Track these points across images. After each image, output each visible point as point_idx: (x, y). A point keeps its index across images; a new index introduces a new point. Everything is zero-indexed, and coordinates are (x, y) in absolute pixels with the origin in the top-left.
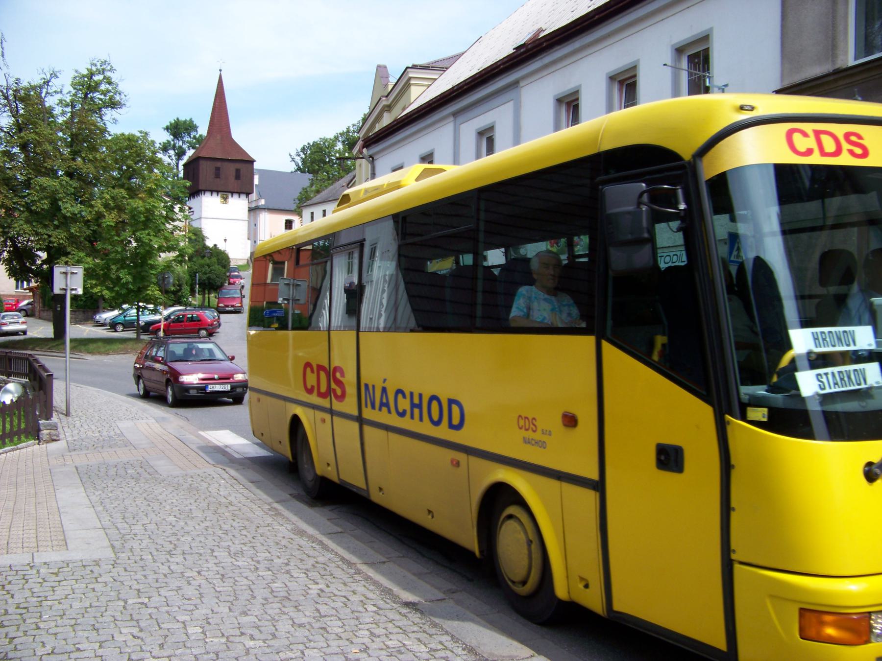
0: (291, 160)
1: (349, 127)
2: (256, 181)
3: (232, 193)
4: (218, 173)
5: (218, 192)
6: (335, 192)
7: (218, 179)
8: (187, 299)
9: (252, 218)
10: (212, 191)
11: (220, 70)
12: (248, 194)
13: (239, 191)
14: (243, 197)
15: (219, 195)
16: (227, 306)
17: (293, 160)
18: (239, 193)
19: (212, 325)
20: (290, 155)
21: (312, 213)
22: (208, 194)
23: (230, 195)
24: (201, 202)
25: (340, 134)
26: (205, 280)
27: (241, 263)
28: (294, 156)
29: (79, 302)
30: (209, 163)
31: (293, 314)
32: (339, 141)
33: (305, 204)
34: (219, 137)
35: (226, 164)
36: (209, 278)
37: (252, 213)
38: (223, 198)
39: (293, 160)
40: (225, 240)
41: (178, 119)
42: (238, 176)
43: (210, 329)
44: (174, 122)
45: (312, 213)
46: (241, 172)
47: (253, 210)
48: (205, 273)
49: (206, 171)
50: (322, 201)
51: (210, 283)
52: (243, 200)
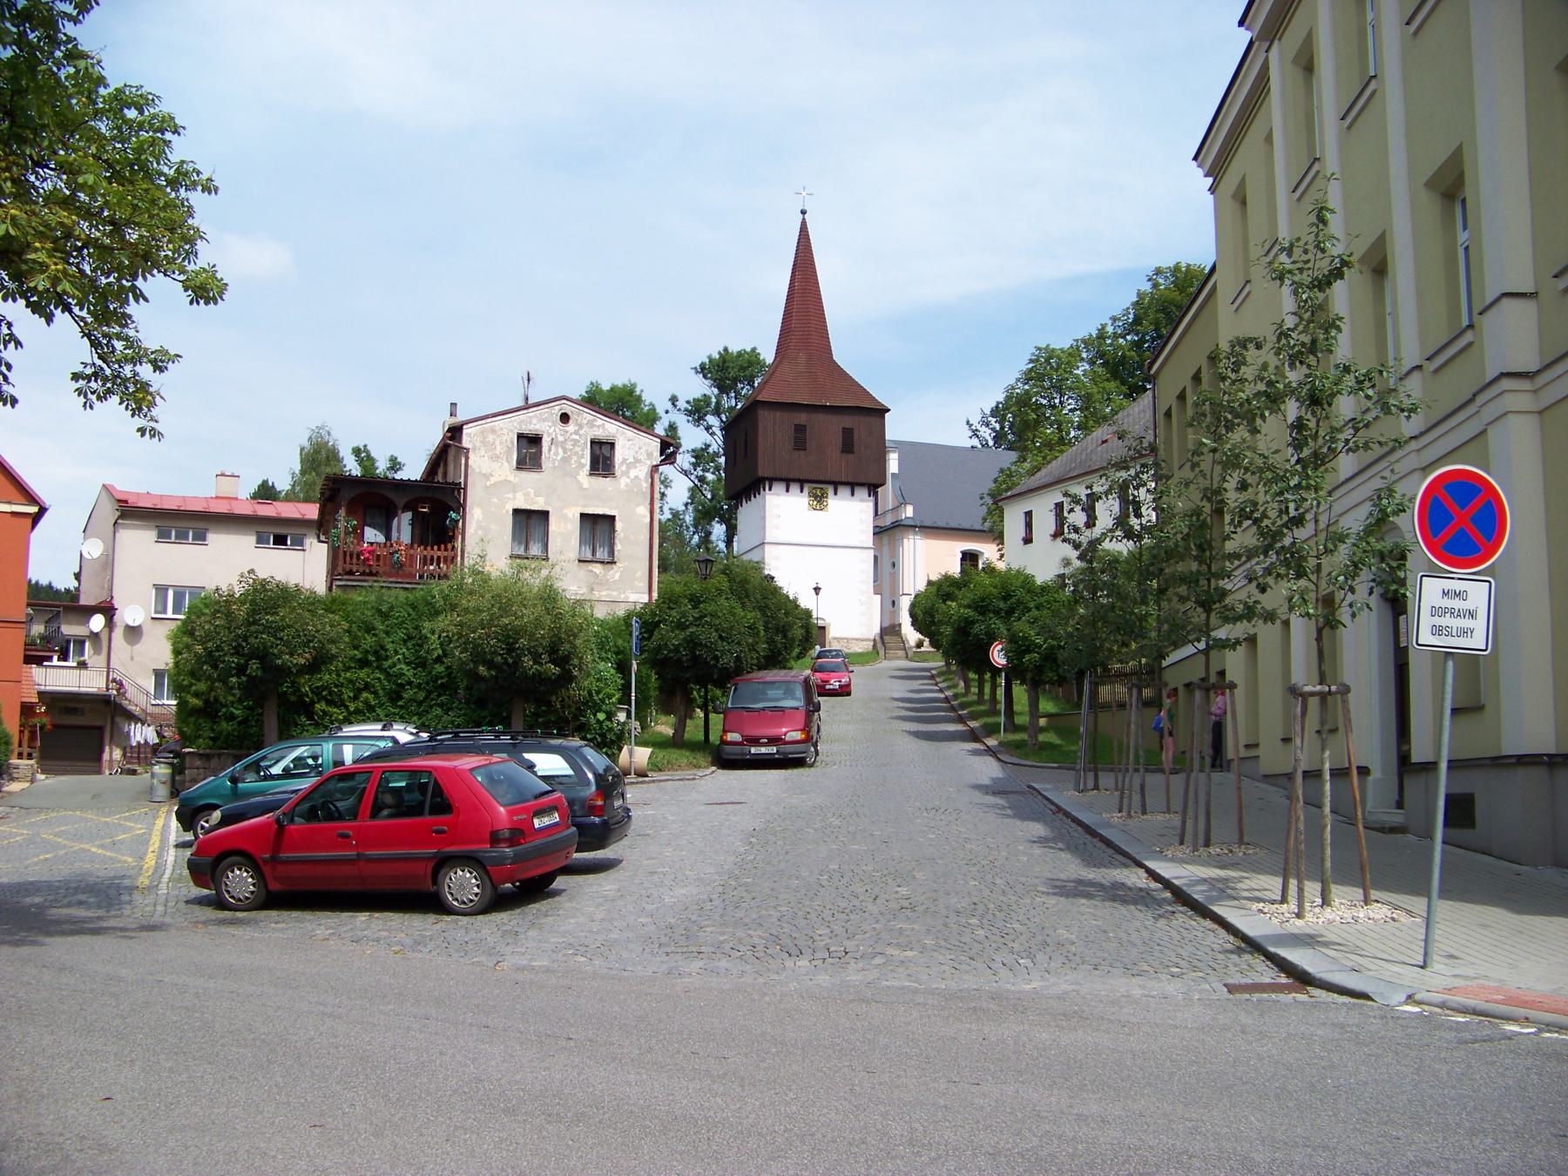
0: (970, 434)
1: (1104, 326)
2: (893, 465)
3: (836, 485)
4: (800, 438)
5: (802, 483)
6: (1084, 457)
7: (802, 453)
8: (610, 716)
9: (886, 549)
10: (788, 482)
11: (803, 212)
12: (873, 488)
13: (850, 480)
14: (862, 493)
15: (806, 490)
16: (755, 741)
17: (975, 433)
18: (853, 486)
19: (520, 833)
20: (968, 423)
21: (1029, 514)
22: (779, 488)
23: (831, 491)
24: (764, 506)
25: (1084, 341)
26: (676, 649)
27: (857, 648)
28: (976, 425)
29: (224, 724)
30: (778, 415)
31: (728, 696)
32: (1083, 359)
33: (1009, 493)
34: (802, 358)
35: (821, 417)
36: (693, 643)
37: (885, 539)
38: (816, 497)
39: (975, 433)
40: (817, 590)
41: (726, 349)
42: (848, 446)
43: (500, 861)
44: (717, 357)
45: (1029, 514)
46: (856, 437)
47: (887, 532)
48: (681, 626)
49: (773, 433)
50: (1051, 480)
51: (695, 659)
52: (861, 500)
